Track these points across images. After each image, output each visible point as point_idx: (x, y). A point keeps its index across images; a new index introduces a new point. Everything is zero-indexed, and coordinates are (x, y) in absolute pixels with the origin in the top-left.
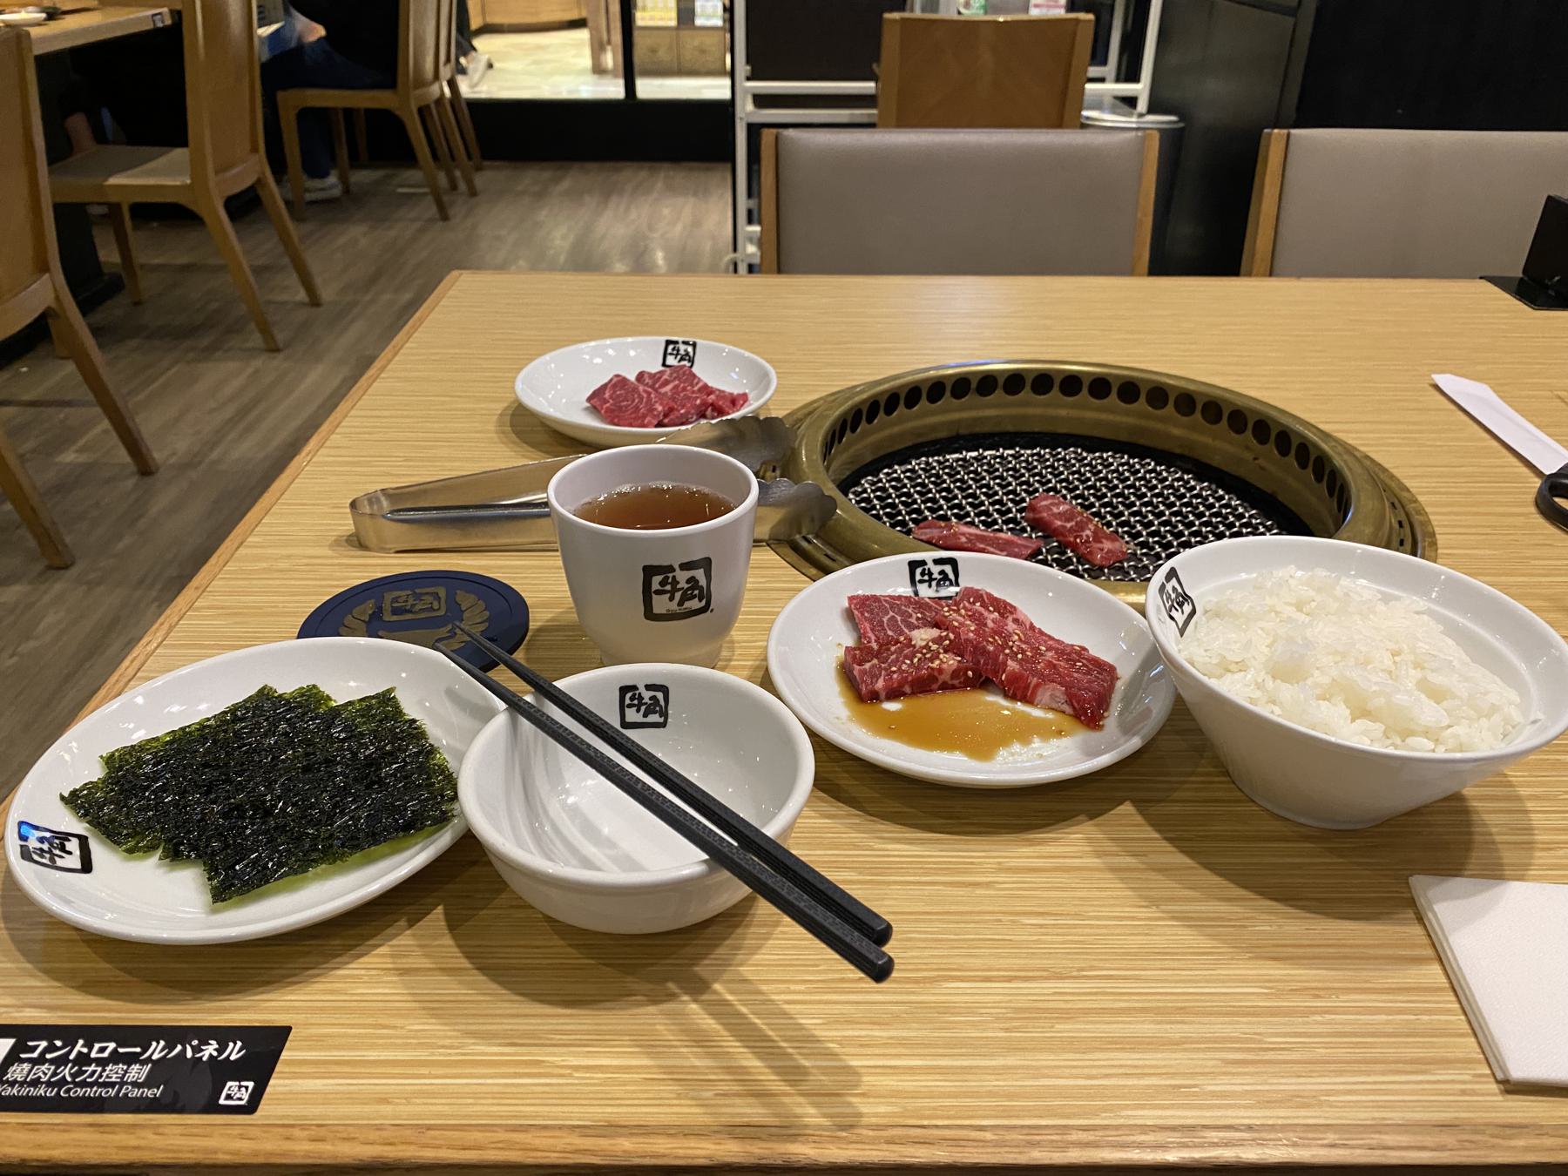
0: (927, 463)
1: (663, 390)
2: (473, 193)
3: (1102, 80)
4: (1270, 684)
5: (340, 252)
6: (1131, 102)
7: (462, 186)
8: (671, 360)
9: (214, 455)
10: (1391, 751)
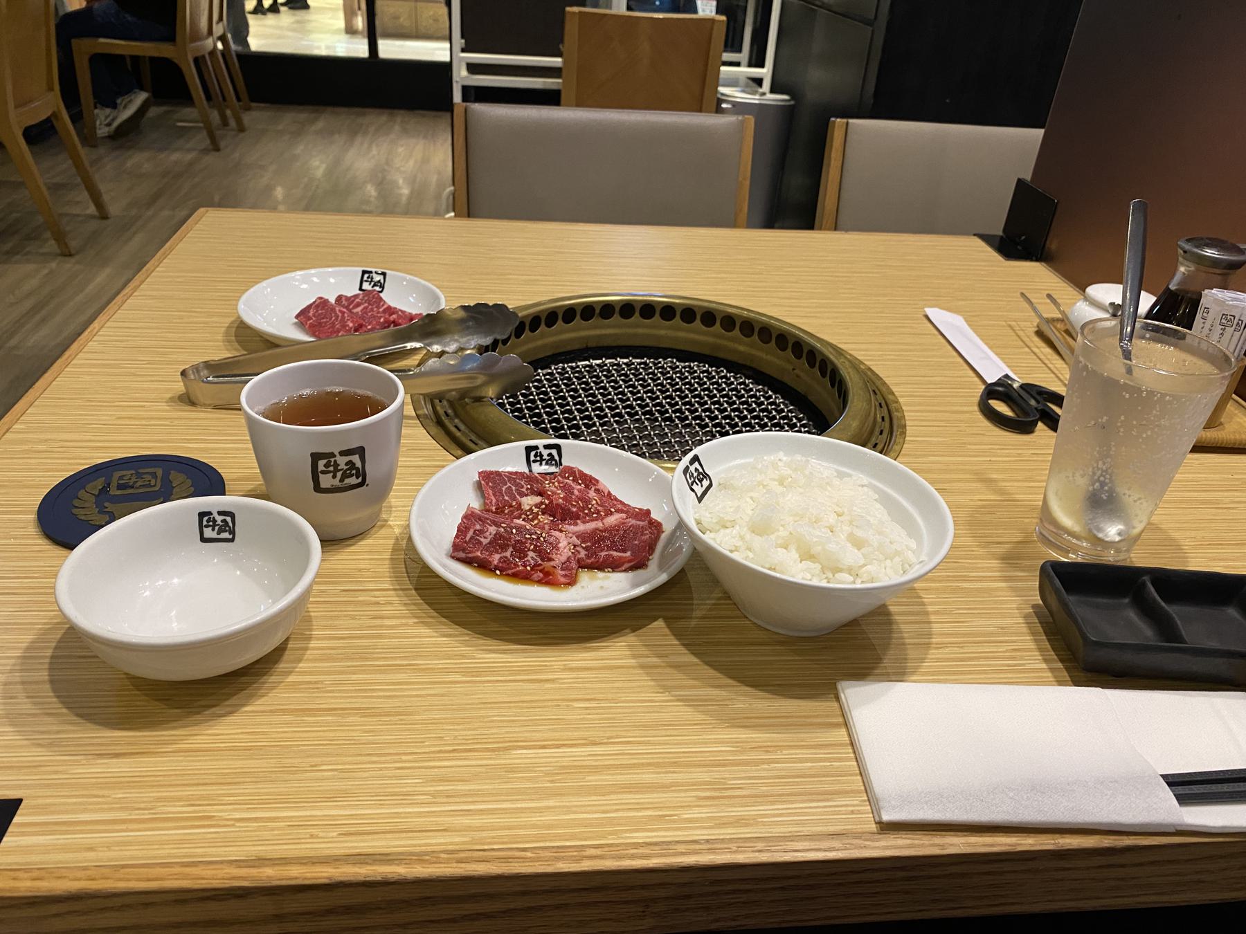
0: (563, 368)
1: (355, 311)
2: (241, 129)
3: (738, 64)
4: (748, 537)
5: (123, 177)
6: (759, 82)
7: (233, 123)
8: (366, 286)
9: (13, 342)
10: (824, 584)
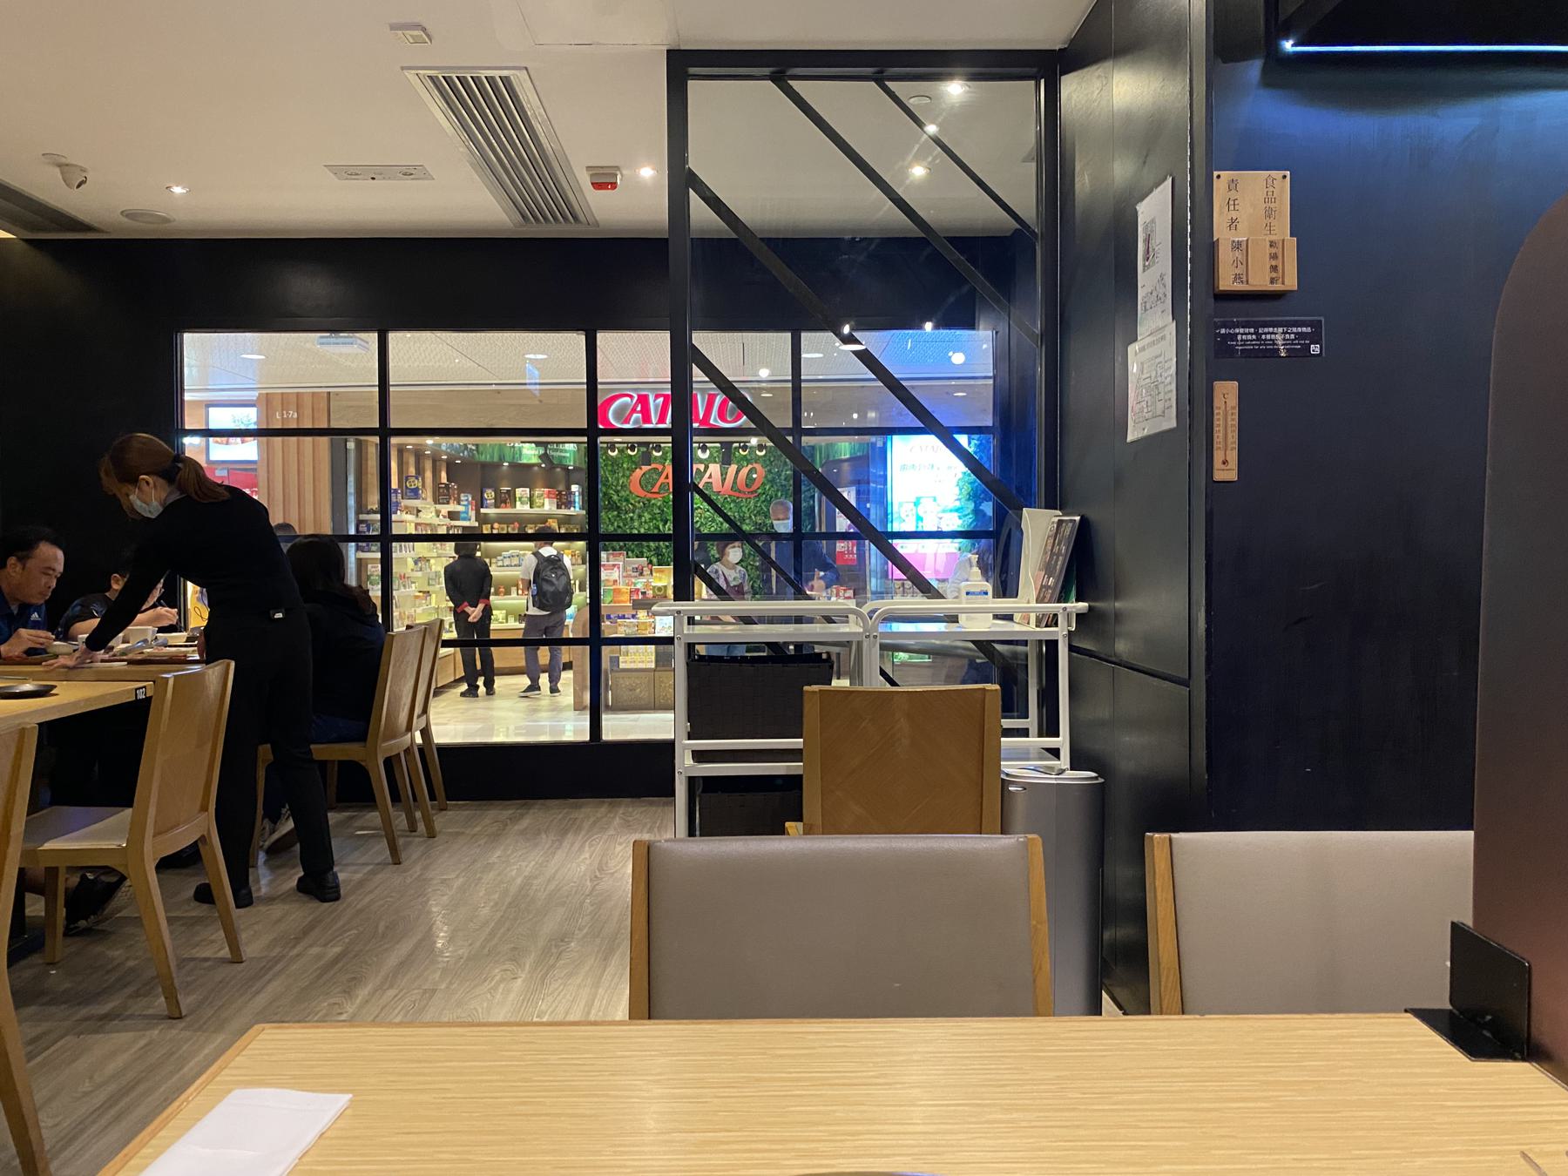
2: (431, 834)
3: (1024, 733)
6: (1055, 753)
7: (421, 827)
